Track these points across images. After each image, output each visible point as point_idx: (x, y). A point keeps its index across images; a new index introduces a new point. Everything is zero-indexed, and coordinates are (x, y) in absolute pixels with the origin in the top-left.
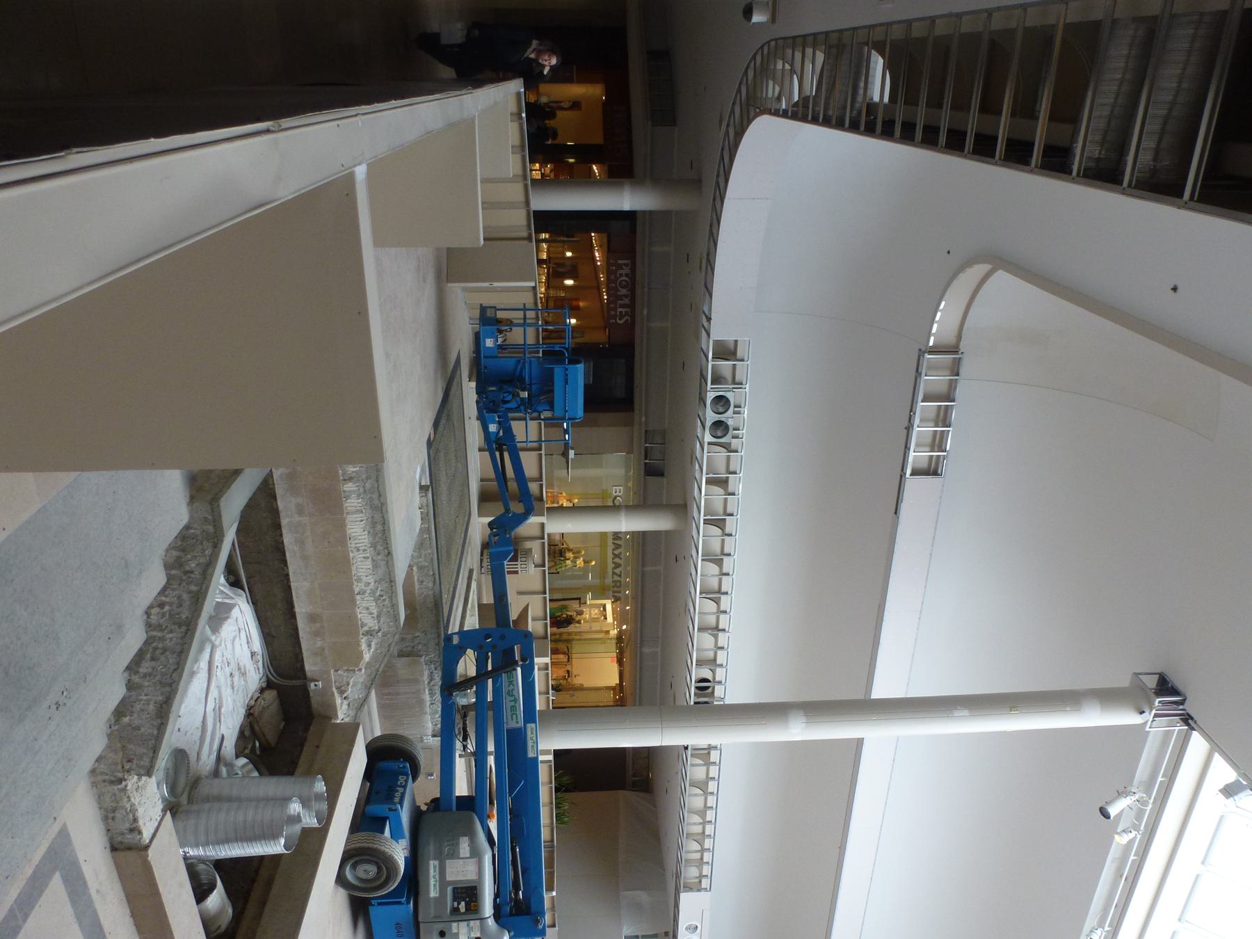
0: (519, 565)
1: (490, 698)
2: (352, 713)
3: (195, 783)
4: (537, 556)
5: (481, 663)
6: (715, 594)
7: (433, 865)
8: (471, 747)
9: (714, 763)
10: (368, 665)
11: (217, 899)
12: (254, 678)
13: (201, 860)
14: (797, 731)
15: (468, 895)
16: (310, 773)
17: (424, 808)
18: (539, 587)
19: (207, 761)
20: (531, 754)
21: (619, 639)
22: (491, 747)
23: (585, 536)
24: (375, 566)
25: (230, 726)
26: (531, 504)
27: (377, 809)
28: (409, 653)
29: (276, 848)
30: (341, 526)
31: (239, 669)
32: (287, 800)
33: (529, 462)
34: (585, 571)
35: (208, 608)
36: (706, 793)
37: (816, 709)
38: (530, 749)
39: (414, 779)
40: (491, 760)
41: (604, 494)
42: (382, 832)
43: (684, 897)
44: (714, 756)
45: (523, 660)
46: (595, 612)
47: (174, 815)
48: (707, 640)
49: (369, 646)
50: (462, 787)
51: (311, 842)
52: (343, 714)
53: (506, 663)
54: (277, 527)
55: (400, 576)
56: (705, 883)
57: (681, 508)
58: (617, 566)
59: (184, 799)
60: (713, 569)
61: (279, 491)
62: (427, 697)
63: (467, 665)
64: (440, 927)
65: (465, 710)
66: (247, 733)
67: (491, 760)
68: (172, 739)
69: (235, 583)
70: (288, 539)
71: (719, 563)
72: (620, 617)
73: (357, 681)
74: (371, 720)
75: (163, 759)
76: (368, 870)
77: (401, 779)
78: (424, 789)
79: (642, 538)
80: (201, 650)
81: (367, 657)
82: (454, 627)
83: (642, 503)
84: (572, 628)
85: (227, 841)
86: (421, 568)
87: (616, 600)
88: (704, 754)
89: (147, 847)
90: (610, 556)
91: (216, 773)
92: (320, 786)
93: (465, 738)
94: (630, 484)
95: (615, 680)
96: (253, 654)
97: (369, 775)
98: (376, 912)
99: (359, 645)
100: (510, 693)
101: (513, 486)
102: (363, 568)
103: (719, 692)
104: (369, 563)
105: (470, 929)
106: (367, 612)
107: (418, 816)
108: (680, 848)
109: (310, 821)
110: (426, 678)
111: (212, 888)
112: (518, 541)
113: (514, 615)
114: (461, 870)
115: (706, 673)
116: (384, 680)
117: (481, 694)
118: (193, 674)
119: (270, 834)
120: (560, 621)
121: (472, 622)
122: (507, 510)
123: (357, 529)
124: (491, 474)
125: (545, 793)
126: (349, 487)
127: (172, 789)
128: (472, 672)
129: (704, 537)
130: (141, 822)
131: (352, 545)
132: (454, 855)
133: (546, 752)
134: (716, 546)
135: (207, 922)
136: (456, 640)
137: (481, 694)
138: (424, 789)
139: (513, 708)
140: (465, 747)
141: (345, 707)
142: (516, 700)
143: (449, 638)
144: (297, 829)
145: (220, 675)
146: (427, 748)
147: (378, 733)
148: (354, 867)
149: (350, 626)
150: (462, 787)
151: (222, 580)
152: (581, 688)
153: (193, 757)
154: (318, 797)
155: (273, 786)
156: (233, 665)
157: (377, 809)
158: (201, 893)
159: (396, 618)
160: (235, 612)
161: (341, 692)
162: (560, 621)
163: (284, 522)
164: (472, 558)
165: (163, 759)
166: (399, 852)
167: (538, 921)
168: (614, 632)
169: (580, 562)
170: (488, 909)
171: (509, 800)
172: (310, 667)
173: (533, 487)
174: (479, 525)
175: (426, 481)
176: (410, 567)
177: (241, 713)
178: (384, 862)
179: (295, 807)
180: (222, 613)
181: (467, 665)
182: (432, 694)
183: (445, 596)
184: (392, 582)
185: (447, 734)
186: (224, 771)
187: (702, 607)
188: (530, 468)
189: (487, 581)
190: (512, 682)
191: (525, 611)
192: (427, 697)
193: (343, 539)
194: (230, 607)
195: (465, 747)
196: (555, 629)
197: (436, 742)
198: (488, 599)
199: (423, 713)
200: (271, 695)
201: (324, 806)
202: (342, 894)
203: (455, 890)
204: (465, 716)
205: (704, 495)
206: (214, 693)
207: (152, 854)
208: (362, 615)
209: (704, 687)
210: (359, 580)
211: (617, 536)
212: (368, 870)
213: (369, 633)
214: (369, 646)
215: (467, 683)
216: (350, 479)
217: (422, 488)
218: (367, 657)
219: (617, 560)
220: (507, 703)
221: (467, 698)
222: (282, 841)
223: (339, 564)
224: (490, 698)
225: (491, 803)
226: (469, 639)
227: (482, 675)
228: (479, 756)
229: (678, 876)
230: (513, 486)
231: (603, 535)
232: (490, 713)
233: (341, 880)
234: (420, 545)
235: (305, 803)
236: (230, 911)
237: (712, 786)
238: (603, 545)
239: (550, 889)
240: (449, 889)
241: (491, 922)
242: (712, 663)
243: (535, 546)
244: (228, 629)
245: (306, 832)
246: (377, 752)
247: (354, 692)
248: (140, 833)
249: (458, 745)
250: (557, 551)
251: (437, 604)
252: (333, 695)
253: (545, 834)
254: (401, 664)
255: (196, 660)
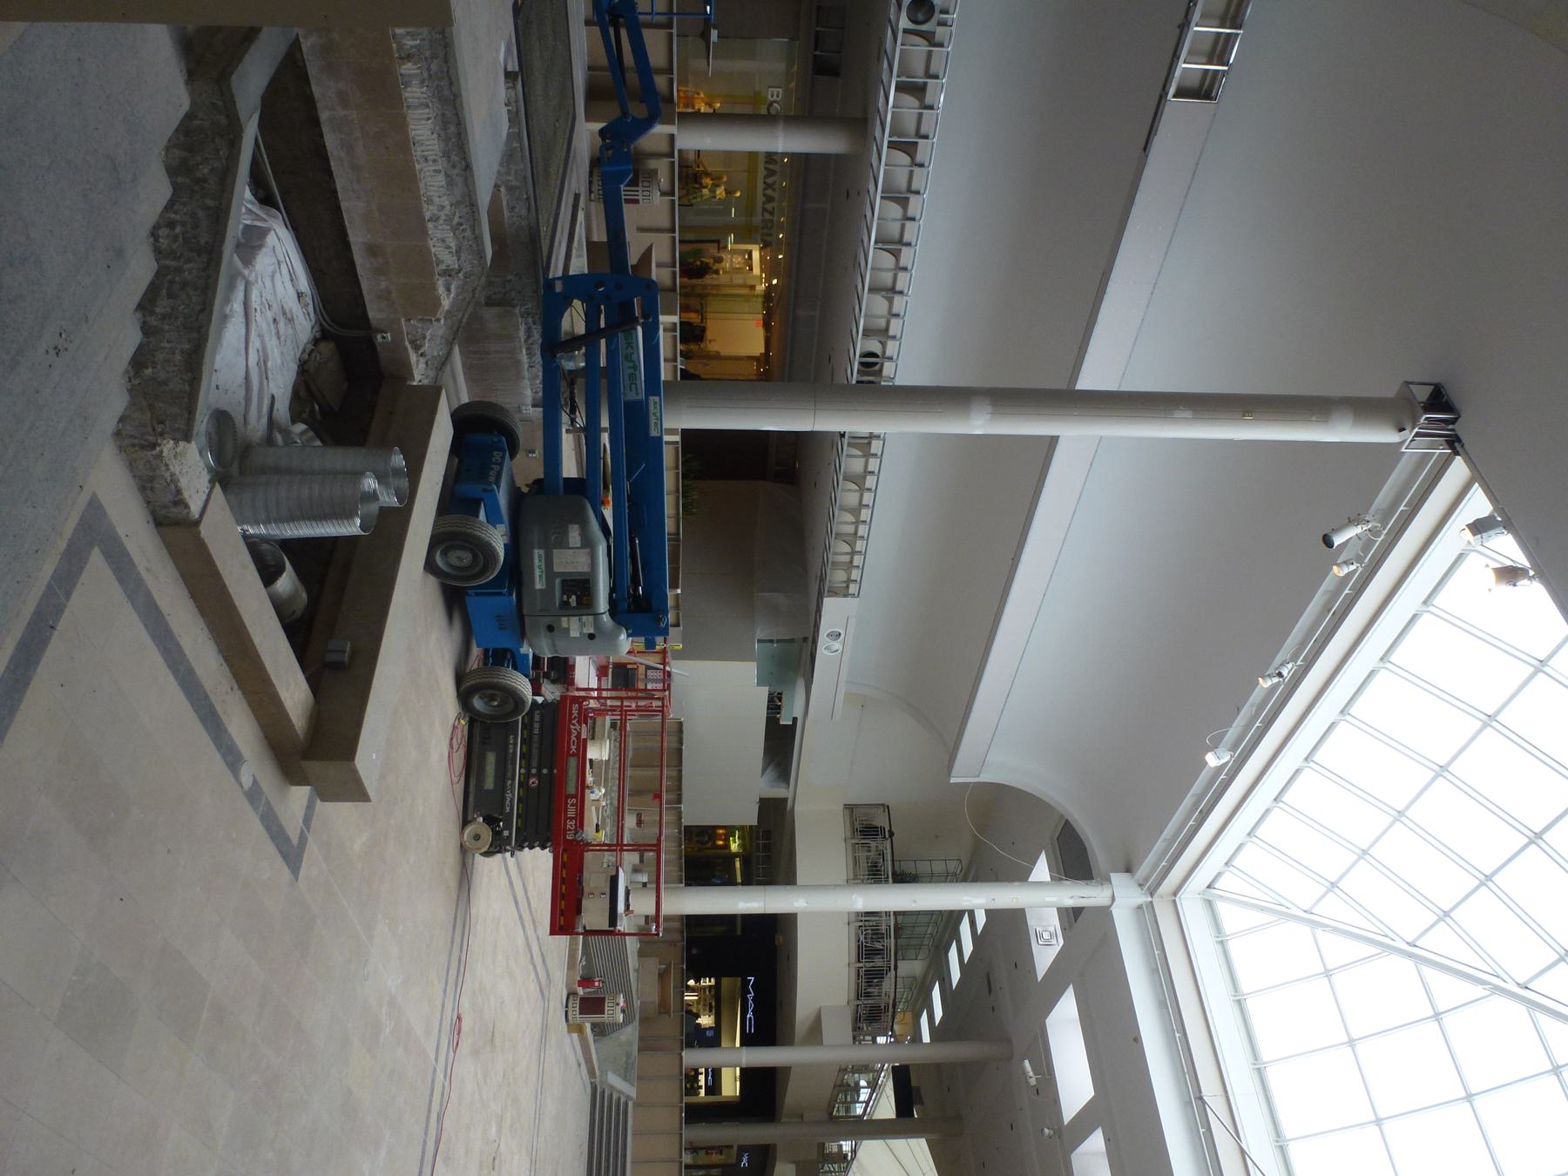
0: (640, 193)
1: (603, 363)
2: (432, 374)
3: (246, 450)
4: (664, 181)
5: (591, 318)
6: (894, 245)
7: (538, 553)
8: (580, 421)
9: (875, 455)
10: (448, 314)
11: (286, 582)
12: (304, 326)
13: (264, 539)
14: (980, 424)
15: (581, 588)
16: (385, 445)
17: (525, 490)
18: (666, 223)
19: (257, 426)
20: (654, 433)
21: (767, 296)
22: (605, 422)
23: (728, 156)
24: (450, 182)
25: (281, 384)
26: (658, 107)
27: (471, 489)
28: (500, 302)
29: (352, 528)
30: (401, 125)
31: (284, 314)
32: (358, 475)
33: (655, 45)
34: (726, 204)
35: (234, 230)
36: (862, 489)
37: (1005, 398)
38: (652, 426)
39: (512, 456)
40: (605, 438)
41: (756, 98)
42: (477, 515)
43: (830, 605)
44: (876, 446)
45: (645, 316)
46: (738, 260)
47: (225, 488)
48: (878, 304)
49: (448, 290)
50: (570, 468)
51: (392, 525)
52: (420, 374)
53: (623, 320)
54: (316, 123)
55: (484, 197)
56: (853, 588)
57: (859, 122)
58: (769, 199)
59: (234, 470)
60: (895, 210)
61: (312, 71)
62: (524, 358)
63: (574, 320)
64: (547, 621)
65: (574, 374)
66: (303, 393)
67: (605, 438)
68: (209, 398)
69: (266, 199)
70: (331, 140)
71: (903, 202)
72: (770, 268)
73: (435, 333)
74: (455, 381)
75: (202, 423)
76: (462, 558)
77: (497, 455)
78: (526, 467)
79: (803, 162)
80: (231, 287)
81: (446, 303)
82: (556, 271)
83: (805, 115)
84: (708, 279)
85: (292, 518)
86: (510, 189)
87: (766, 246)
88: (864, 443)
89: (197, 523)
90: (760, 185)
91: (269, 440)
92: (398, 460)
93: (573, 410)
94: (793, 85)
95: (758, 348)
96: (300, 295)
97: (457, 448)
98: (472, 602)
99: (434, 287)
100: (628, 358)
101: (632, 78)
102: (433, 183)
103: (888, 369)
104: (441, 180)
105: (583, 625)
106: (442, 245)
107: (517, 498)
108: (827, 549)
109: (389, 499)
110: (522, 334)
111: (280, 571)
112: (640, 157)
113: (633, 258)
114: (570, 561)
115: (874, 346)
116: (468, 333)
117: (592, 357)
118: (225, 318)
119: (346, 515)
120: (694, 268)
121: (579, 265)
122: (625, 113)
123: (423, 130)
124: (603, 60)
125: (669, 480)
126: (408, 68)
127: (219, 457)
128: (580, 329)
129: (887, 165)
130: (186, 495)
131: (417, 152)
132: (563, 543)
133: (672, 432)
134: (901, 180)
135: (280, 606)
136: (559, 287)
137: (592, 357)
138: (526, 467)
139: (633, 377)
140: (573, 421)
141: (422, 366)
142: (636, 367)
143: (549, 284)
144: (374, 508)
145: (261, 320)
146: (526, 420)
147: (465, 399)
148: (444, 553)
149: (422, 264)
150: (570, 468)
151: (248, 194)
152: (717, 357)
153: (239, 419)
154: (397, 472)
155: (340, 458)
156: (275, 307)
157: (471, 489)
158: (269, 575)
159: (481, 254)
160: (271, 239)
161: (417, 348)
162: (694, 268)
163: (324, 116)
164: (578, 179)
165: (202, 423)
166: (498, 539)
167: (660, 620)
168: (761, 288)
169: (720, 192)
170: (603, 604)
171: (627, 485)
172: (374, 313)
173: (660, 82)
174: (587, 133)
175: (513, 66)
176: (497, 186)
177: (294, 367)
178: (482, 550)
179: (370, 483)
180: (252, 242)
181: (574, 320)
182: (530, 354)
183: (543, 229)
184: (473, 206)
185: (550, 404)
186: (279, 438)
187: (875, 259)
188: (656, 57)
189: (598, 210)
190: (631, 344)
191: (647, 256)
192: (524, 358)
193: (405, 145)
194: (263, 233)
195: (573, 421)
196: (685, 280)
197: (536, 413)
198: (600, 235)
199: (519, 377)
200: (327, 348)
201: (404, 483)
202: (432, 581)
203: (564, 582)
204: (572, 384)
205: (892, 103)
206: (255, 343)
207: (204, 530)
208: (436, 249)
209: (871, 363)
210: (430, 201)
211: (771, 157)
212: (462, 558)
213: (448, 273)
214: (448, 290)
215: (574, 342)
216: (409, 57)
217: (509, 76)
218: (446, 303)
219: (769, 192)
220: (624, 369)
221: (575, 362)
222: (358, 521)
223: (403, 179)
224: (603, 363)
225: (606, 487)
226: (575, 286)
227: (593, 333)
228: (591, 432)
229: (822, 580)
230: (632, 78)
231: (752, 156)
232: (604, 382)
233: (430, 566)
234: (509, 158)
235: (381, 478)
236: (304, 595)
237: (870, 482)
238: (752, 171)
239: (674, 586)
240: (558, 581)
241: (606, 618)
242: (883, 334)
243: (661, 166)
244: (263, 262)
245: (385, 512)
246: (465, 421)
247: (432, 347)
248: (187, 506)
249: (565, 418)
250: (691, 174)
251: (533, 239)
252: (406, 349)
253: (669, 526)
254: (489, 313)
255: (227, 300)
